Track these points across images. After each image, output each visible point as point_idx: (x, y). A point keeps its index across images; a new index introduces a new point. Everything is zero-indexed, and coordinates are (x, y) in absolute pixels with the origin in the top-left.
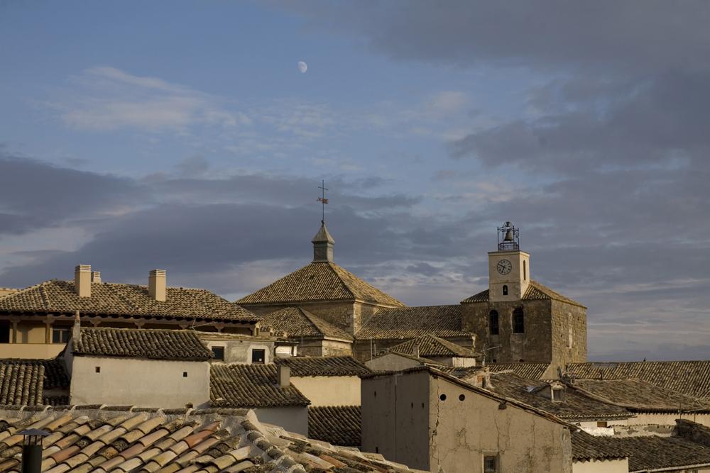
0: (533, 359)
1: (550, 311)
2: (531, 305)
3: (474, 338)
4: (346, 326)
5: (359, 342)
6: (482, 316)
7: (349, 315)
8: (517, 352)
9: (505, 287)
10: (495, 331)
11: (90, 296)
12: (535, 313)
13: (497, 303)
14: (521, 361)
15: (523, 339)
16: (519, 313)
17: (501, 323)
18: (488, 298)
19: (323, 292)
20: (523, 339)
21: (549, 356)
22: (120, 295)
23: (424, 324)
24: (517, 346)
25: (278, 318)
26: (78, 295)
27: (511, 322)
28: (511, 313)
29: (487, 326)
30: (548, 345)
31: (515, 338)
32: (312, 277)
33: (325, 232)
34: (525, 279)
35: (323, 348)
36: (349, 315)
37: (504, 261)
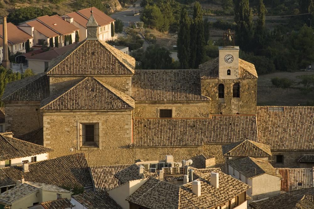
0: (245, 113)
2: (245, 82)
4: (125, 90)
8: (235, 108)
9: (229, 71)
10: (221, 95)
12: (247, 86)
13: (224, 80)
15: (239, 101)
17: (225, 92)
20: (239, 101)
24: (236, 105)
26: (197, 196)
29: (217, 92)
31: (234, 101)
32: (93, 53)
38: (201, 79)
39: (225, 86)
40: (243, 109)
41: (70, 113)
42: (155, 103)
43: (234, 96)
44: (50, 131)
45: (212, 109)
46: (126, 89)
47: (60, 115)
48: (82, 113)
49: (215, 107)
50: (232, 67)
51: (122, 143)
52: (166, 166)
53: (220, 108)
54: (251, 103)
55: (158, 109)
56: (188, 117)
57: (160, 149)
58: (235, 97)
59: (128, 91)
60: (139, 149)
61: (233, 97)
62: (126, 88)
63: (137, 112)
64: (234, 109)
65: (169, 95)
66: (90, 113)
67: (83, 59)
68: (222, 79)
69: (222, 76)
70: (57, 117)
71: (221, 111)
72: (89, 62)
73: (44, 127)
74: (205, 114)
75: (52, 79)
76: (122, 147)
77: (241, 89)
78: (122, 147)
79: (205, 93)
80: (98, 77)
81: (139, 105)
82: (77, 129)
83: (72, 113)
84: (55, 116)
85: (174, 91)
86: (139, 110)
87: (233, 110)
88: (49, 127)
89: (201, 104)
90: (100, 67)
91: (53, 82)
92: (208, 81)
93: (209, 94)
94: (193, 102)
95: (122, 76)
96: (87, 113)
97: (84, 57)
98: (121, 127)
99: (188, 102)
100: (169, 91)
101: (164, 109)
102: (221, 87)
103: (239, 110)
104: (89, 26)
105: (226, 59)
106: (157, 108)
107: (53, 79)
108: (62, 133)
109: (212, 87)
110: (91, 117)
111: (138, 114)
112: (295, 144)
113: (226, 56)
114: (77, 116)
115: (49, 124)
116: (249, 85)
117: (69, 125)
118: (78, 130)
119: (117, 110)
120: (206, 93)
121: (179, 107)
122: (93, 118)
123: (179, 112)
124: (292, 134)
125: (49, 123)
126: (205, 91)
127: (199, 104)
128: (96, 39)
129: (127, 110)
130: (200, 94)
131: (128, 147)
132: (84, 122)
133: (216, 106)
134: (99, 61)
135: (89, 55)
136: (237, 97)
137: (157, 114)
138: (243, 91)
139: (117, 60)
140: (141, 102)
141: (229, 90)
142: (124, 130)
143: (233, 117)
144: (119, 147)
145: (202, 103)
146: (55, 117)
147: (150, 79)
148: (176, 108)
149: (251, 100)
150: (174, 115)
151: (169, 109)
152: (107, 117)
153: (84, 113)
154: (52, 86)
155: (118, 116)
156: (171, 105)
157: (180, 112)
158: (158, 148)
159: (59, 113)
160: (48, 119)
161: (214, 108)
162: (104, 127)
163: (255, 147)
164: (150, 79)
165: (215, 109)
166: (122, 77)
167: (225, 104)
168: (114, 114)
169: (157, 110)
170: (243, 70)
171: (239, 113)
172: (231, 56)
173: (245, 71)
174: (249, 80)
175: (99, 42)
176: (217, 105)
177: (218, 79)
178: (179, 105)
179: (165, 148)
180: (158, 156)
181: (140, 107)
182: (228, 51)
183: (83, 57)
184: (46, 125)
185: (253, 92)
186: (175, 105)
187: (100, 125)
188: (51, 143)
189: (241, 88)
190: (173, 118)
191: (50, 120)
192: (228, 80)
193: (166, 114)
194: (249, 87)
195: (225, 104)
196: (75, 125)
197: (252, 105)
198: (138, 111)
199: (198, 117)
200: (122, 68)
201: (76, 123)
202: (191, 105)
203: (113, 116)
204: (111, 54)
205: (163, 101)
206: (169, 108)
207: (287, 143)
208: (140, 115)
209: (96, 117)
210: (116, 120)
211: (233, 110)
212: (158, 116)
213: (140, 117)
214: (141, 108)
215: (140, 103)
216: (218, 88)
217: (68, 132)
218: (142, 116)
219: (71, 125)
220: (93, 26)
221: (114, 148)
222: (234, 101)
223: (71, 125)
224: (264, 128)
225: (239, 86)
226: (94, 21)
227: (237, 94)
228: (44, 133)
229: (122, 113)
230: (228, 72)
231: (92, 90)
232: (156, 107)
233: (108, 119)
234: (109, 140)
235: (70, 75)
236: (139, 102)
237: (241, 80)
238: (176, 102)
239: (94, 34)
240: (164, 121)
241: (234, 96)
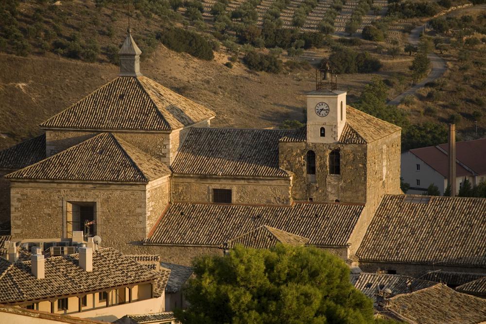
0: (348, 200)
1: (365, 155)
2: (348, 148)
3: (291, 178)
4: (161, 156)
5: (176, 175)
6: (298, 155)
7: (165, 145)
8: (333, 192)
9: (322, 129)
10: (312, 170)
11: (44, 278)
12: (351, 156)
13: (315, 145)
14: (337, 201)
15: (339, 180)
16: (336, 155)
17: (317, 164)
18: (305, 138)
19: (136, 118)
20: (339, 180)
21: (363, 198)
22: (63, 272)
23: (241, 155)
24: (333, 187)
25: (93, 149)
26: (36, 278)
27: (328, 163)
28: (327, 154)
29: (304, 165)
30: (363, 187)
31: (331, 179)
32: (121, 97)
33: (131, 43)
34: (342, 119)
35: (147, 192)
36: (165, 145)
37: (322, 103)
38: (279, 142)
39: (316, 155)
40: (345, 193)
41: (52, 184)
42: (204, 177)
43: (331, 172)
44: (20, 213)
45: (297, 192)
46: (163, 154)
47: (36, 188)
48: (70, 185)
49: (301, 189)
50: (327, 124)
51: (132, 236)
52: (70, 245)
53: (310, 191)
54: (357, 185)
55: (211, 188)
56: (257, 203)
57: (191, 248)
58: (333, 174)
59: (165, 157)
60: (158, 247)
61: (330, 173)
62: (163, 152)
63: (178, 192)
64: (332, 194)
65: (229, 167)
66: (82, 186)
67: (103, 105)
68: (312, 143)
69: (313, 137)
70: (32, 191)
71: (311, 195)
72: (112, 109)
73: (13, 206)
74: (283, 200)
75: (50, 135)
76: (133, 243)
77: (341, 160)
78: (133, 243)
79: (285, 165)
80: (120, 132)
81: (181, 180)
82: (62, 210)
83: (55, 185)
84: (29, 189)
85: (240, 160)
86: (181, 188)
87: (329, 194)
88: (19, 206)
89: (277, 183)
90: (126, 117)
91: (51, 139)
92: (290, 145)
93: (291, 167)
94: (263, 178)
95: (157, 133)
96: (78, 185)
97: (106, 102)
98: (130, 211)
99: (255, 178)
100: (233, 160)
101: (219, 188)
102: (311, 156)
103: (339, 196)
104: (123, 53)
105: (317, 109)
106: (208, 187)
107: (52, 135)
108: (40, 216)
109: (297, 155)
110: (84, 192)
111: (180, 195)
112: (417, 253)
113: (318, 105)
114: (62, 190)
115: (20, 202)
116: (354, 154)
117: (51, 205)
118: (65, 213)
119: (123, 183)
120: (287, 166)
121: (243, 186)
122: (88, 196)
123: (243, 195)
124: (422, 237)
125: (19, 200)
126: (285, 161)
127: (274, 183)
128: (134, 75)
129: (138, 183)
130: (278, 167)
131: (141, 243)
132: (74, 201)
133: (302, 187)
134: (127, 108)
135: (114, 99)
136: (335, 174)
137: (209, 196)
138: (345, 163)
139: (156, 107)
140: (182, 175)
141: (324, 160)
142: (136, 215)
143: (328, 205)
144: (128, 243)
145: (279, 181)
146: (28, 191)
147: (212, 142)
148: (239, 188)
149: (359, 179)
150: (234, 198)
151: (226, 188)
152: (108, 192)
153: (74, 186)
154: (50, 145)
155: (126, 192)
156: (230, 182)
157: (244, 194)
158: (188, 248)
159: (36, 184)
160: (18, 193)
161: (300, 190)
162: (105, 209)
163: (270, 237)
164: (212, 142)
165: (301, 192)
166: (156, 135)
167: (317, 185)
168: (119, 188)
169: (209, 190)
170: (351, 130)
171: (339, 199)
172: (328, 108)
173: (352, 132)
174: (355, 145)
175: (137, 79)
176: (304, 185)
177: (306, 142)
178: (242, 182)
179: (199, 248)
180: (189, 261)
181: (183, 184)
182: (321, 96)
183: (104, 102)
184: (14, 203)
185: (360, 165)
186: (237, 182)
187: (98, 206)
188: (22, 233)
189: (342, 158)
190: (233, 204)
191: (22, 195)
192: (322, 145)
193: (223, 197)
194: (355, 158)
195: (317, 185)
196: (60, 205)
197: (360, 187)
198: (180, 191)
199: (272, 204)
200: (158, 120)
201: (61, 201)
202: (261, 182)
203: (118, 192)
204: (149, 98)
205: (216, 175)
206: (228, 188)
207: (405, 251)
208: (182, 197)
209: (91, 193)
210: (122, 199)
211: (329, 194)
212: (211, 200)
213: (183, 200)
214: (185, 185)
215: (182, 177)
216: (306, 158)
217: (49, 215)
218: (185, 198)
219: (53, 205)
220: (129, 53)
221: (119, 244)
222: (331, 179)
223: (53, 205)
224: (382, 226)
225: (339, 154)
226: (131, 45)
227: (336, 169)
228: (12, 215)
229: (132, 188)
230: (321, 131)
231: (101, 153)
232: (207, 185)
233: (110, 197)
234: (112, 232)
235: (76, 129)
236: (180, 175)
237: (342, 145)
238: (237, 177)
239: (131, 66)
240: (217, 209)
241: (331, 172)
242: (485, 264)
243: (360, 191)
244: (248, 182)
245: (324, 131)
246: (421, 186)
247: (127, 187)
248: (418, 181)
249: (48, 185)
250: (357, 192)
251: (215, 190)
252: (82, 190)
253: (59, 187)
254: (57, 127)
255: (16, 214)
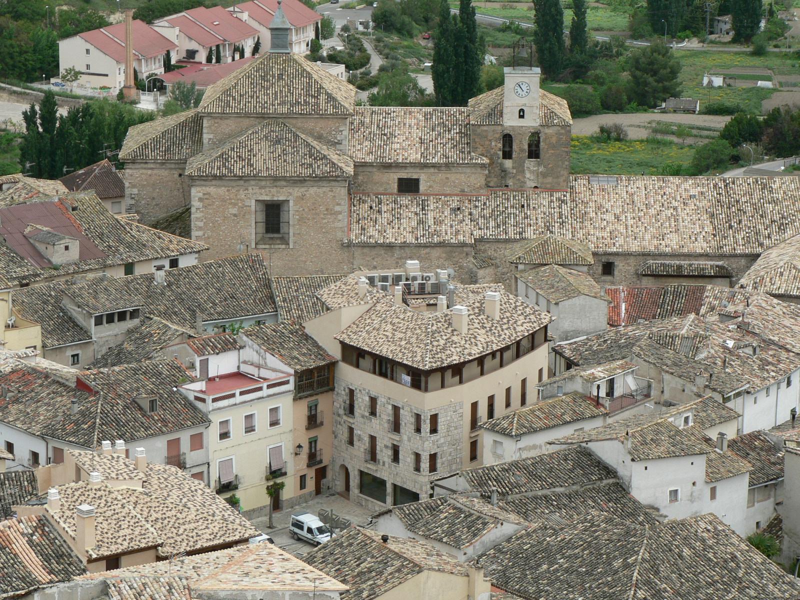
0: (548, 186)
9: (522, 110)
15: (539, 165)
24: (532, 172)
32: (280, 77)
47: (219, 186)
84: (212, 188)
102: (507, 139)
125: (200, 200)
141: (521, 145)
153: (263, 183)
156: (418, 170)
178: (432, 170)
186: (425, 170)
187: (291, 203)
206: (415, 177)
211: (527, 180)
217: (235, 215)
230: (520, 113)
242: (663, 598)
243: (563, 175)
244: (439, 170)
245: (523, 113)
246: (91, 71)
247: (325, 184)
248: (88, 67)
249: (234, 184)
250: (558, 177)
251: (400, 180)
252: (273, 187)
253: (246, 184)
254: (219, 113)
255: (198, 215)
